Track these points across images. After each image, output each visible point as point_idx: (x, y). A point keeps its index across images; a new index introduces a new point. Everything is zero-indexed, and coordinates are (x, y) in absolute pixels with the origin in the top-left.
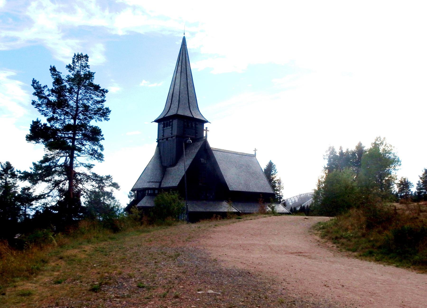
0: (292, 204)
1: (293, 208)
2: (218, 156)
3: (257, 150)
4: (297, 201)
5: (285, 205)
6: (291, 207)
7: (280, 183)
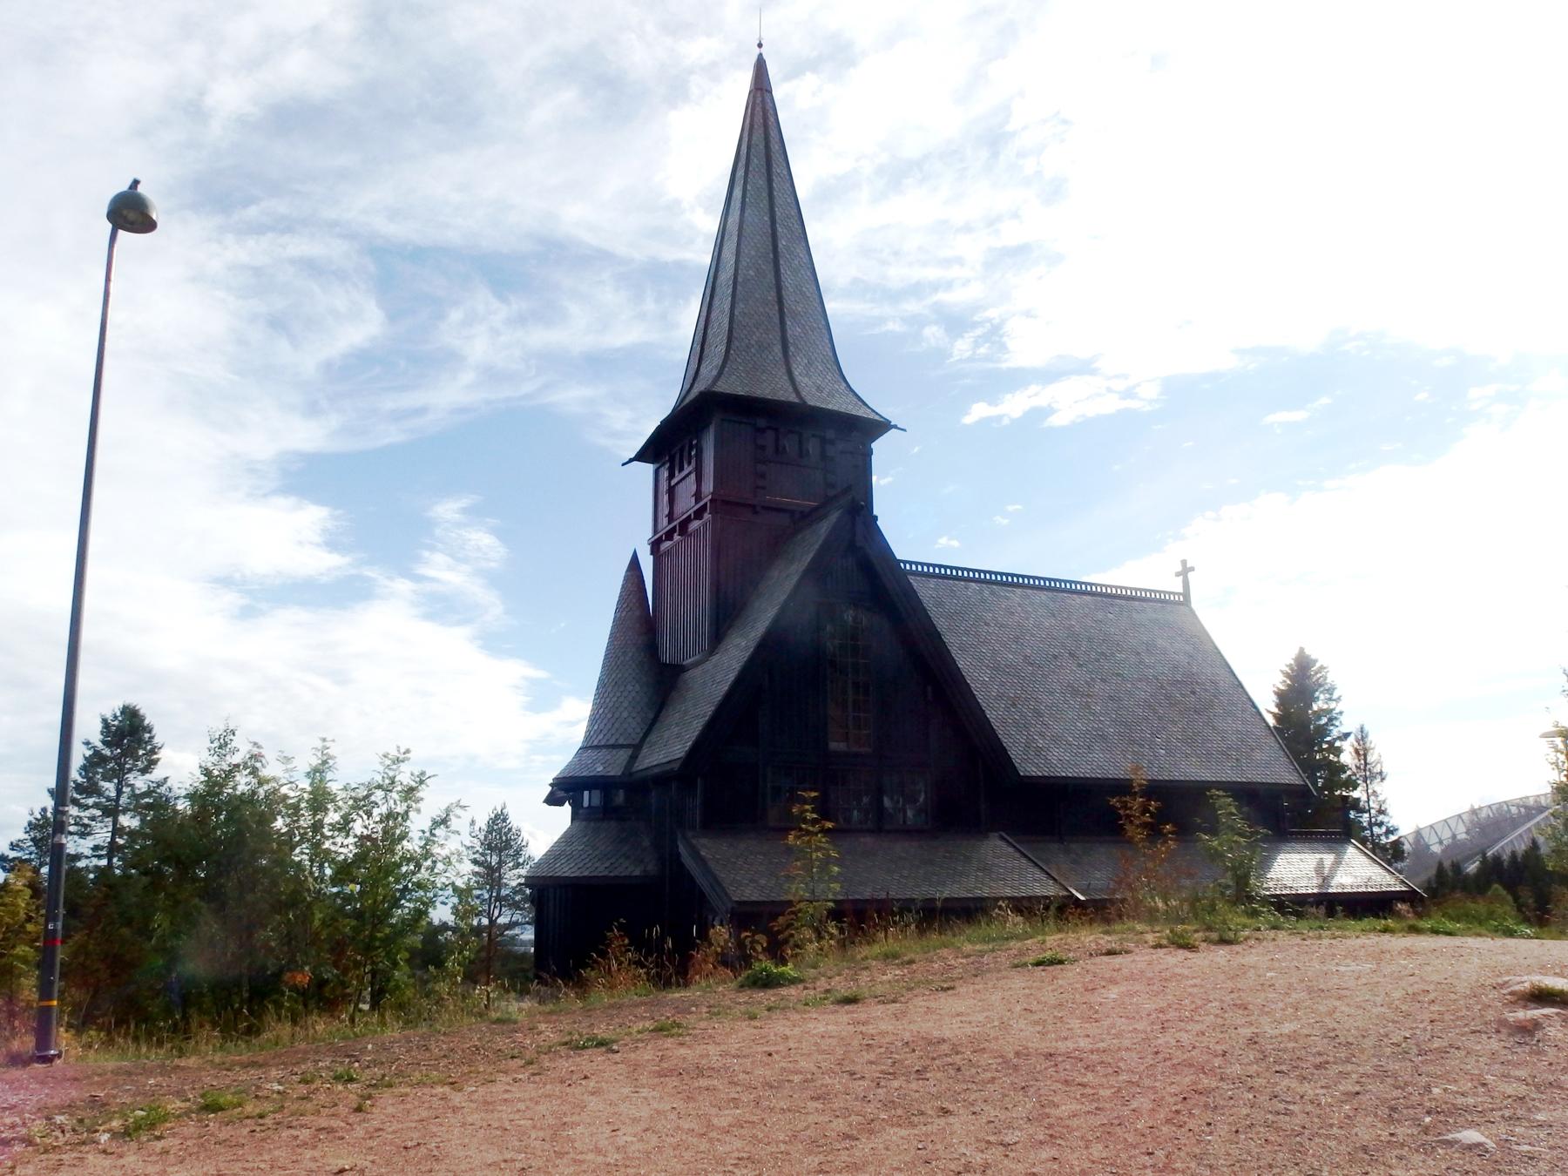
0: (1443, 851)
1: (1447, 864)
2: (926, 592)
3: (1192, 569)
4: (1462, 836)
5: (1390, 854)
6: (1440, 865)
7: (1365, 755)
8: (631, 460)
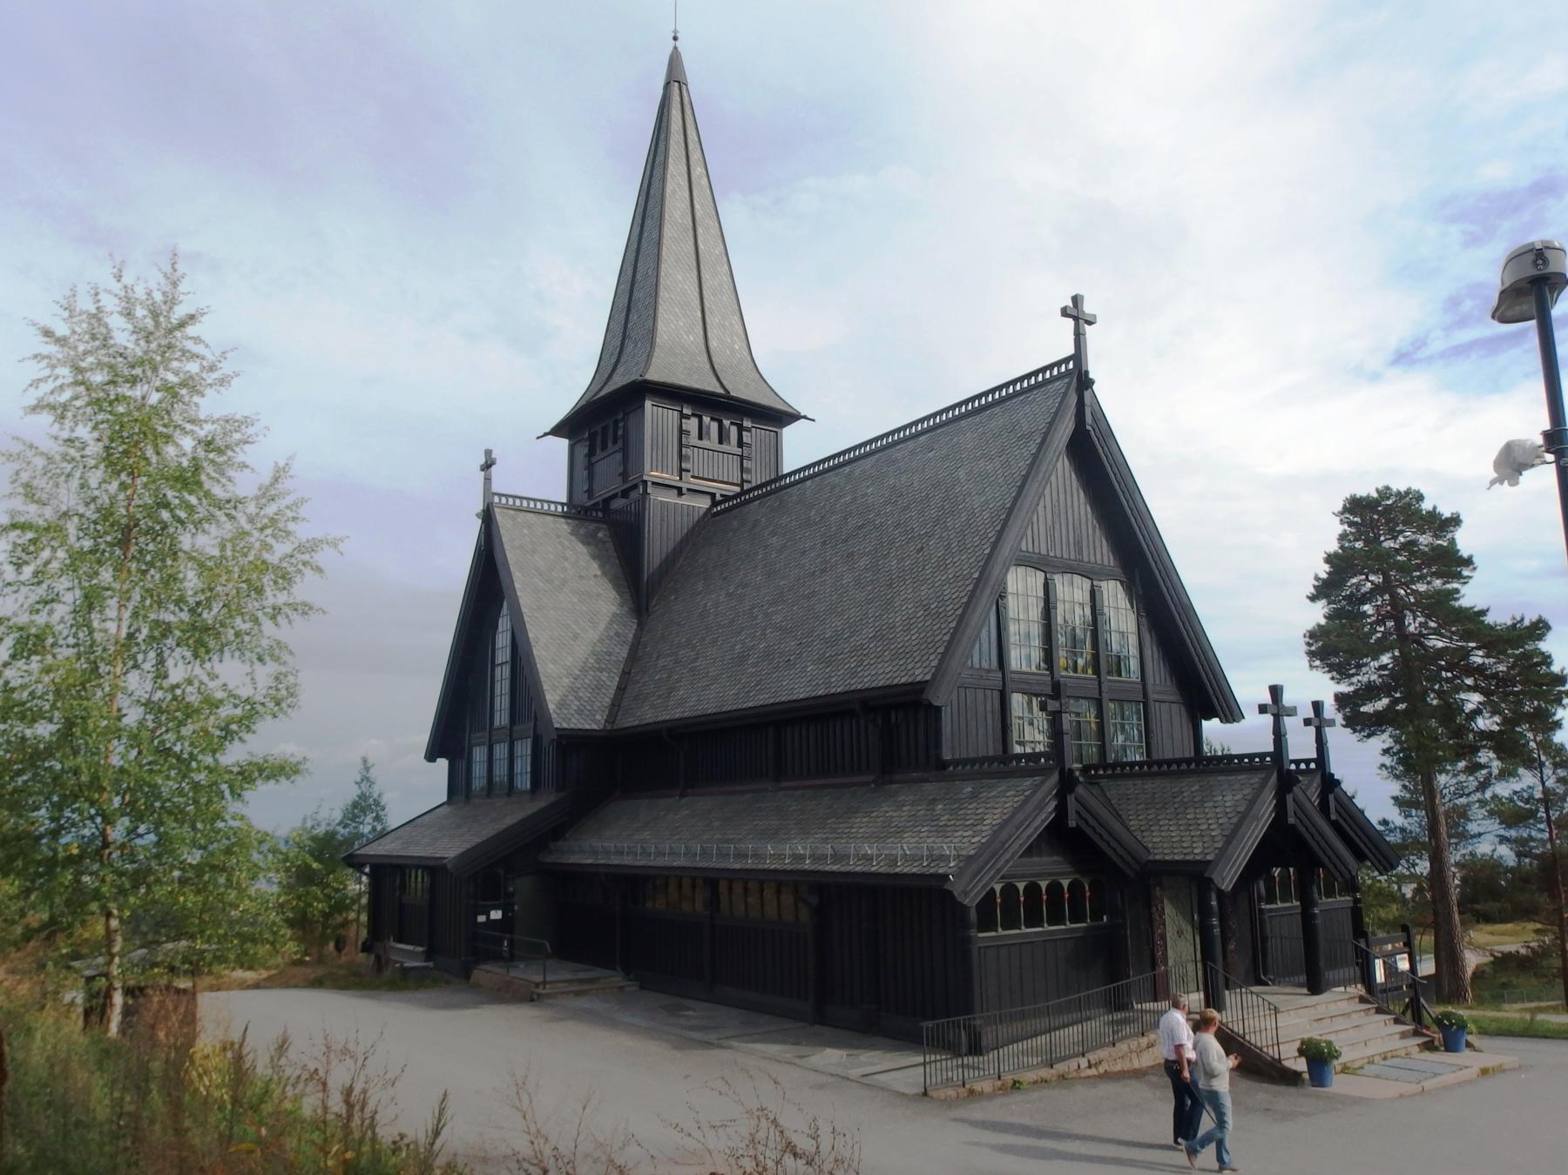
8: (546, 434)
